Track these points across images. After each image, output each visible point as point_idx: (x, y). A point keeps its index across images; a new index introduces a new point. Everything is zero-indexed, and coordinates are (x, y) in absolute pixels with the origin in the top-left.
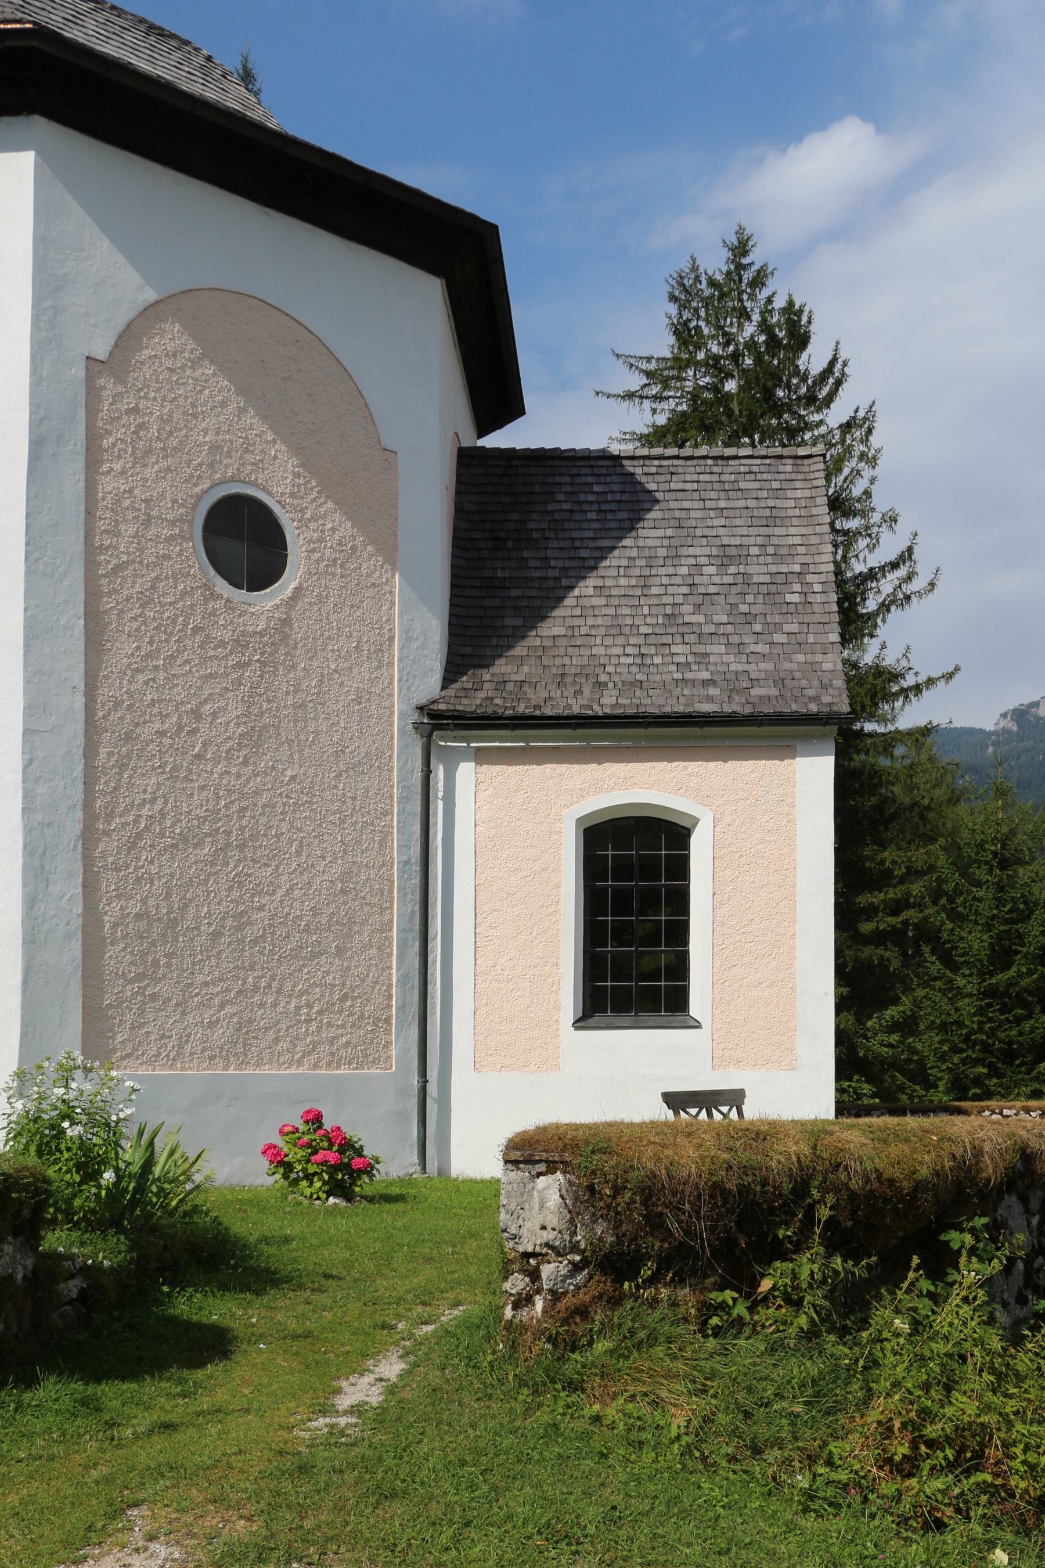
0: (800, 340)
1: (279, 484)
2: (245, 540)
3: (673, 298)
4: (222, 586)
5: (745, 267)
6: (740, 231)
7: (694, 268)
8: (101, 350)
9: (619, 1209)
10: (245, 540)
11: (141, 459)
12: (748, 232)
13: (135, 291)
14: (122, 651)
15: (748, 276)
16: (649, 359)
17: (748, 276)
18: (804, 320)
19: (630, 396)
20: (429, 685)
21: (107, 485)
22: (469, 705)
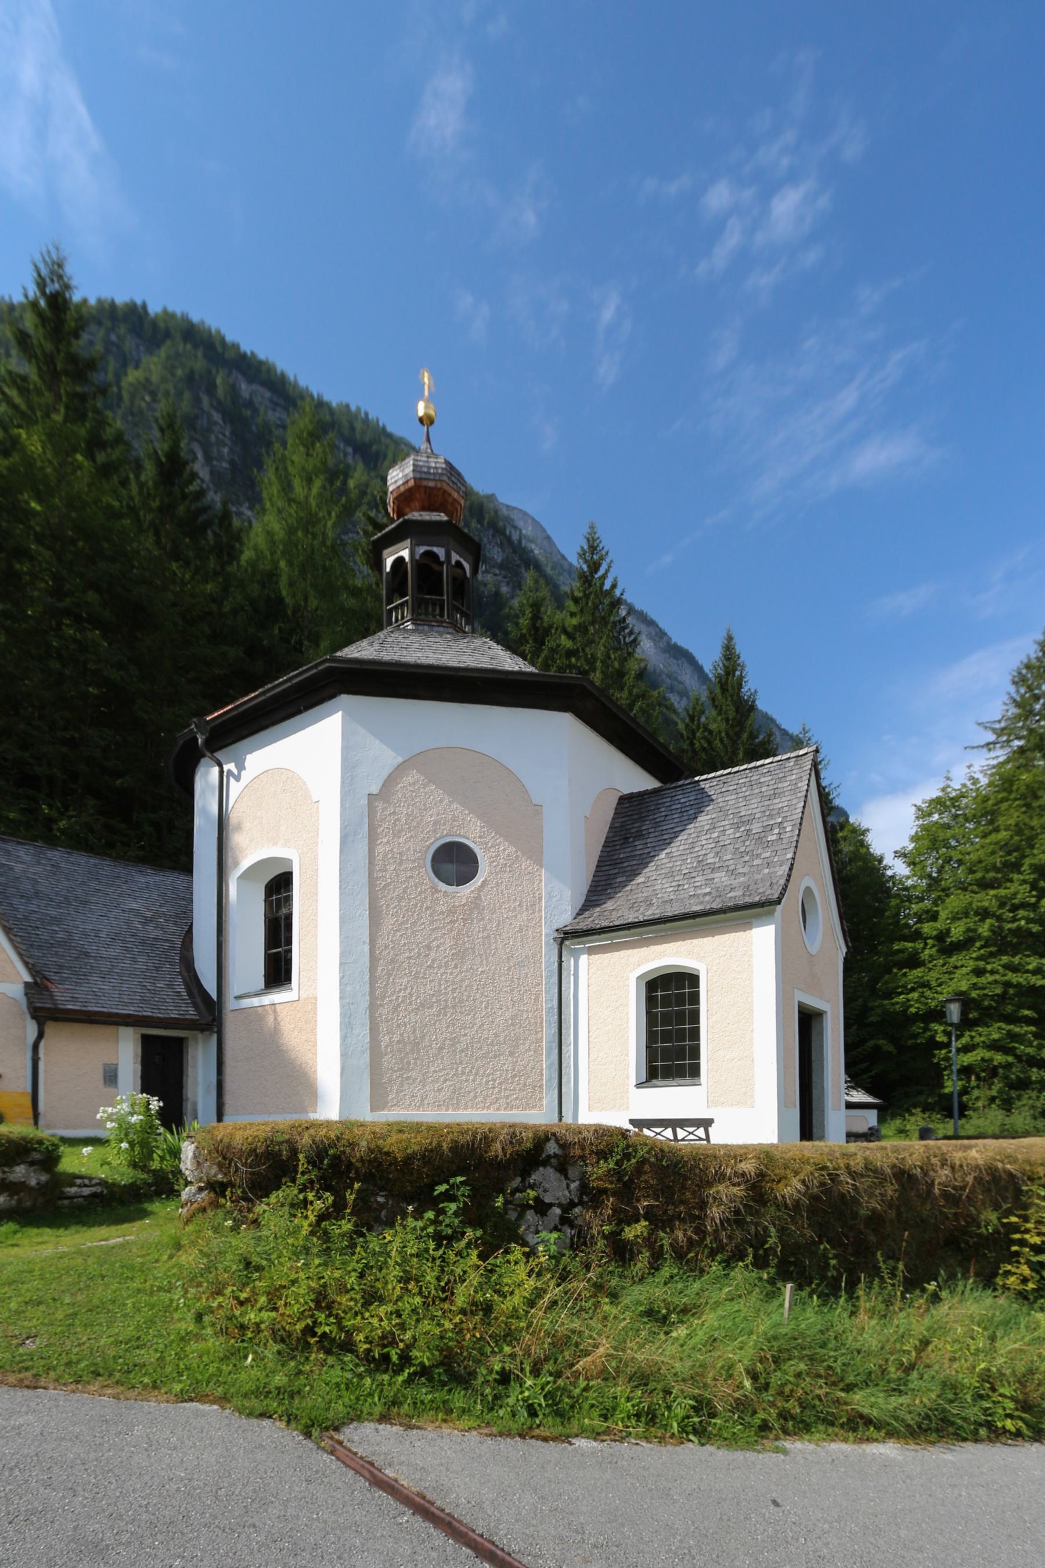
1: (472, 833)
4: (443, 886)
10: (455, 862)
11: (397, 835)
13: (391, 759)
14: (388, 923)
21: (380, 849)
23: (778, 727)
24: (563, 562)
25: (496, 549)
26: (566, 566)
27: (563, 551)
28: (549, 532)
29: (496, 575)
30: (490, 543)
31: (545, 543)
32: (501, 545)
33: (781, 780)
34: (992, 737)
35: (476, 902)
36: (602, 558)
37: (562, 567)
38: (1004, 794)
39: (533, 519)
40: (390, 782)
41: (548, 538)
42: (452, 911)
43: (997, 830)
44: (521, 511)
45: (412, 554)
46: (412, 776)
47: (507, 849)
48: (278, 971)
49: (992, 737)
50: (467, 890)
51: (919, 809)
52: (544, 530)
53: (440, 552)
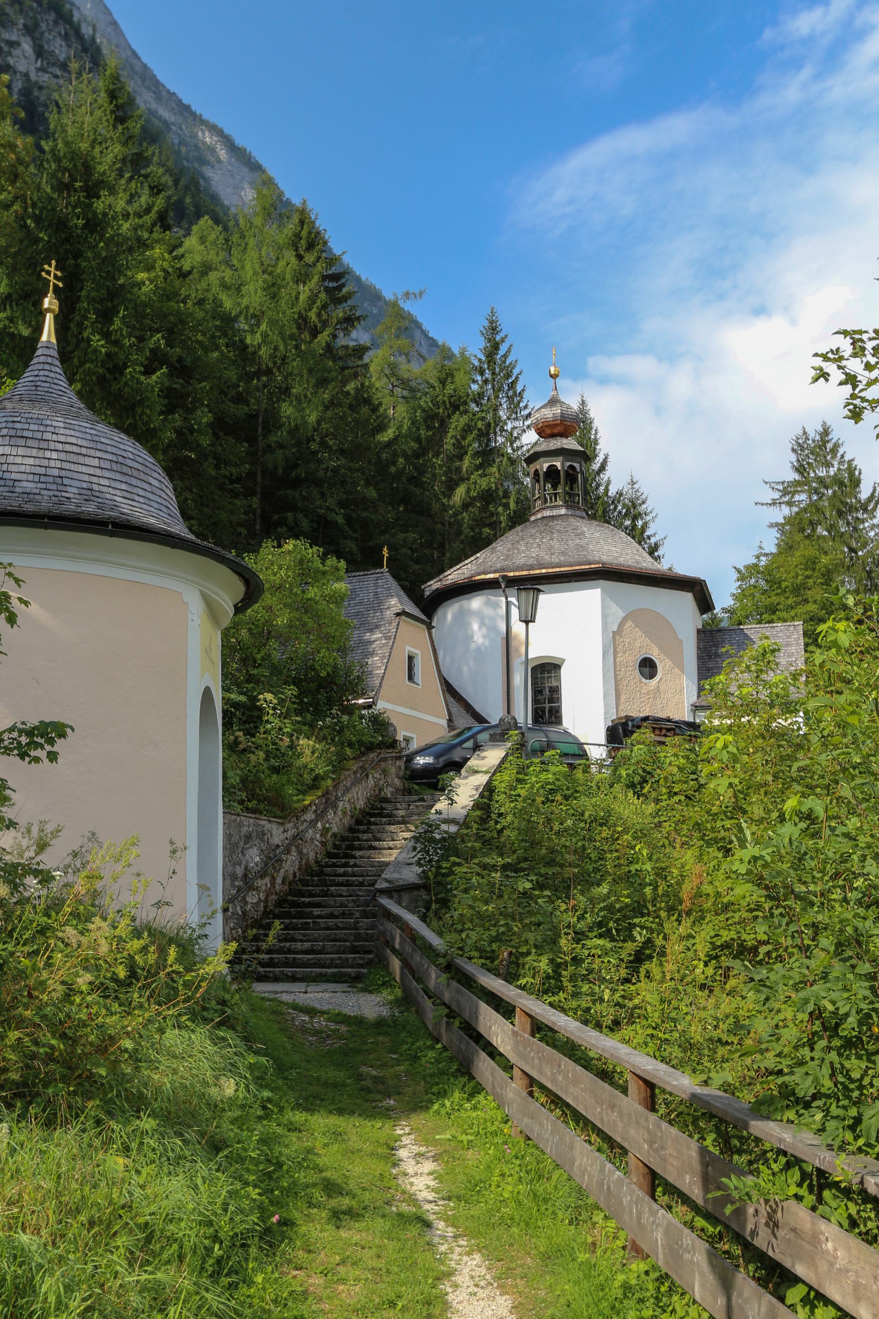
0: (856, 482)
1: (655, 654)
2: (648, 667)
3: (793, 450)
4: (644, 680)
5: (828, 441)
6: (824, 424)
7: (805, 433)
8: (615, 629)
9: (509, 546)
10: (648, 667)
11: (625, 653)
12: (828, 424)
13: (621, 614)
14: (623, 698)
15: (829, 446)
16: (783, 483)
17: (829, 446)
18: (857, 473)
19: (774, 503)
20: (694, 699)
21: (618, 660)
22: (704, 703)
23: (425, 334)
24: (134, 61)
25: (59, 41)
26: (138, 67)
27: (134, 46)
28: (117, 16)
29: (56, 76)
30: (50, 31)
32: (66, 37)
33: (789, 637)
34: (777, 495)
36: (503, 340)
37: (132, 67)
38: (809, 573)
41: (114, 24)
42: (648, 693)
43: (806, 601)
45: (563, 465)
46: (629, 623)
47: (669, 663)
49: (777, 495)
50: (654, 682)
51: (739, 571)
52: (108, 12)
53: (577, 466)
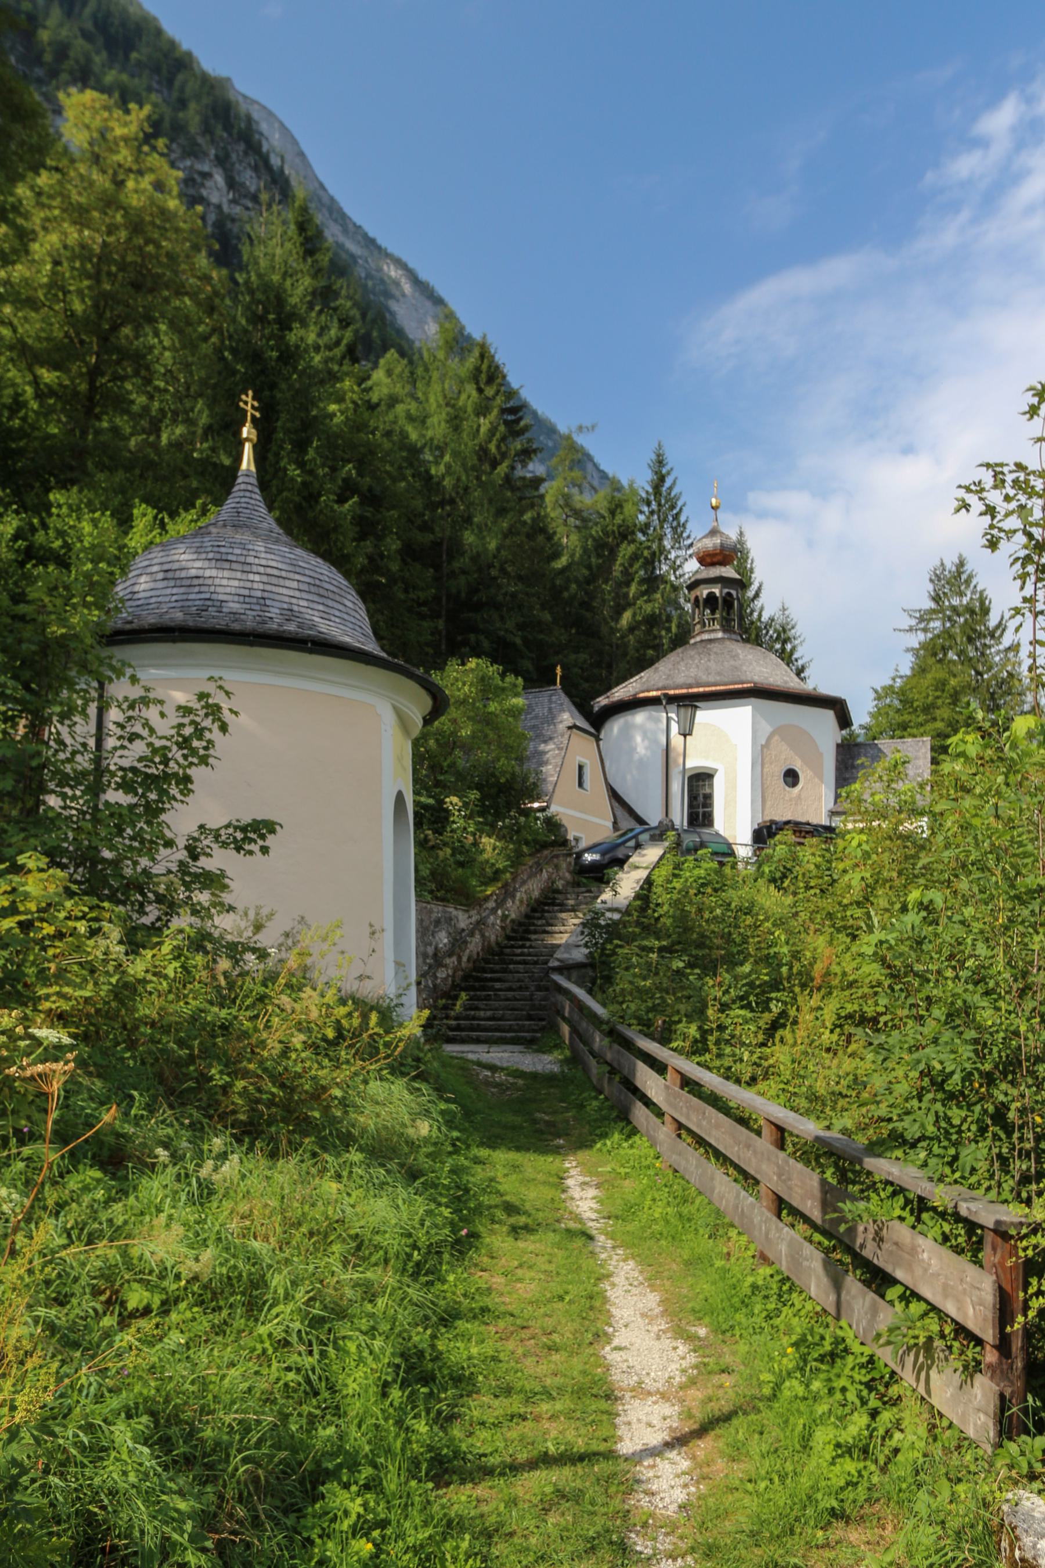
1: (798, 766)
10: (791, 777)
14: (769, 804)
23: (596, 466)
24: (321, 193)
29: (247, 209)
31: (297, 160)
32: (256, 169)
34: (913, 622)
35: (799, 797)
37: (320, 200)
39: (282, 124)
40: (769, 739)
41: (302, 154)
43: (935, 719)
44: (264, 108)
47: (810, 773)
48: (400, 797)
49: (913, 622)
52: (295, 142)
